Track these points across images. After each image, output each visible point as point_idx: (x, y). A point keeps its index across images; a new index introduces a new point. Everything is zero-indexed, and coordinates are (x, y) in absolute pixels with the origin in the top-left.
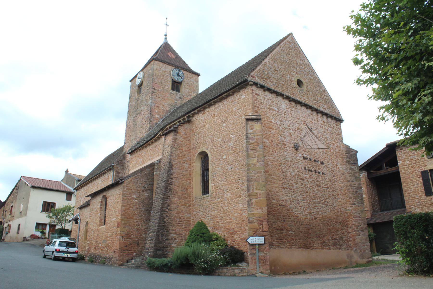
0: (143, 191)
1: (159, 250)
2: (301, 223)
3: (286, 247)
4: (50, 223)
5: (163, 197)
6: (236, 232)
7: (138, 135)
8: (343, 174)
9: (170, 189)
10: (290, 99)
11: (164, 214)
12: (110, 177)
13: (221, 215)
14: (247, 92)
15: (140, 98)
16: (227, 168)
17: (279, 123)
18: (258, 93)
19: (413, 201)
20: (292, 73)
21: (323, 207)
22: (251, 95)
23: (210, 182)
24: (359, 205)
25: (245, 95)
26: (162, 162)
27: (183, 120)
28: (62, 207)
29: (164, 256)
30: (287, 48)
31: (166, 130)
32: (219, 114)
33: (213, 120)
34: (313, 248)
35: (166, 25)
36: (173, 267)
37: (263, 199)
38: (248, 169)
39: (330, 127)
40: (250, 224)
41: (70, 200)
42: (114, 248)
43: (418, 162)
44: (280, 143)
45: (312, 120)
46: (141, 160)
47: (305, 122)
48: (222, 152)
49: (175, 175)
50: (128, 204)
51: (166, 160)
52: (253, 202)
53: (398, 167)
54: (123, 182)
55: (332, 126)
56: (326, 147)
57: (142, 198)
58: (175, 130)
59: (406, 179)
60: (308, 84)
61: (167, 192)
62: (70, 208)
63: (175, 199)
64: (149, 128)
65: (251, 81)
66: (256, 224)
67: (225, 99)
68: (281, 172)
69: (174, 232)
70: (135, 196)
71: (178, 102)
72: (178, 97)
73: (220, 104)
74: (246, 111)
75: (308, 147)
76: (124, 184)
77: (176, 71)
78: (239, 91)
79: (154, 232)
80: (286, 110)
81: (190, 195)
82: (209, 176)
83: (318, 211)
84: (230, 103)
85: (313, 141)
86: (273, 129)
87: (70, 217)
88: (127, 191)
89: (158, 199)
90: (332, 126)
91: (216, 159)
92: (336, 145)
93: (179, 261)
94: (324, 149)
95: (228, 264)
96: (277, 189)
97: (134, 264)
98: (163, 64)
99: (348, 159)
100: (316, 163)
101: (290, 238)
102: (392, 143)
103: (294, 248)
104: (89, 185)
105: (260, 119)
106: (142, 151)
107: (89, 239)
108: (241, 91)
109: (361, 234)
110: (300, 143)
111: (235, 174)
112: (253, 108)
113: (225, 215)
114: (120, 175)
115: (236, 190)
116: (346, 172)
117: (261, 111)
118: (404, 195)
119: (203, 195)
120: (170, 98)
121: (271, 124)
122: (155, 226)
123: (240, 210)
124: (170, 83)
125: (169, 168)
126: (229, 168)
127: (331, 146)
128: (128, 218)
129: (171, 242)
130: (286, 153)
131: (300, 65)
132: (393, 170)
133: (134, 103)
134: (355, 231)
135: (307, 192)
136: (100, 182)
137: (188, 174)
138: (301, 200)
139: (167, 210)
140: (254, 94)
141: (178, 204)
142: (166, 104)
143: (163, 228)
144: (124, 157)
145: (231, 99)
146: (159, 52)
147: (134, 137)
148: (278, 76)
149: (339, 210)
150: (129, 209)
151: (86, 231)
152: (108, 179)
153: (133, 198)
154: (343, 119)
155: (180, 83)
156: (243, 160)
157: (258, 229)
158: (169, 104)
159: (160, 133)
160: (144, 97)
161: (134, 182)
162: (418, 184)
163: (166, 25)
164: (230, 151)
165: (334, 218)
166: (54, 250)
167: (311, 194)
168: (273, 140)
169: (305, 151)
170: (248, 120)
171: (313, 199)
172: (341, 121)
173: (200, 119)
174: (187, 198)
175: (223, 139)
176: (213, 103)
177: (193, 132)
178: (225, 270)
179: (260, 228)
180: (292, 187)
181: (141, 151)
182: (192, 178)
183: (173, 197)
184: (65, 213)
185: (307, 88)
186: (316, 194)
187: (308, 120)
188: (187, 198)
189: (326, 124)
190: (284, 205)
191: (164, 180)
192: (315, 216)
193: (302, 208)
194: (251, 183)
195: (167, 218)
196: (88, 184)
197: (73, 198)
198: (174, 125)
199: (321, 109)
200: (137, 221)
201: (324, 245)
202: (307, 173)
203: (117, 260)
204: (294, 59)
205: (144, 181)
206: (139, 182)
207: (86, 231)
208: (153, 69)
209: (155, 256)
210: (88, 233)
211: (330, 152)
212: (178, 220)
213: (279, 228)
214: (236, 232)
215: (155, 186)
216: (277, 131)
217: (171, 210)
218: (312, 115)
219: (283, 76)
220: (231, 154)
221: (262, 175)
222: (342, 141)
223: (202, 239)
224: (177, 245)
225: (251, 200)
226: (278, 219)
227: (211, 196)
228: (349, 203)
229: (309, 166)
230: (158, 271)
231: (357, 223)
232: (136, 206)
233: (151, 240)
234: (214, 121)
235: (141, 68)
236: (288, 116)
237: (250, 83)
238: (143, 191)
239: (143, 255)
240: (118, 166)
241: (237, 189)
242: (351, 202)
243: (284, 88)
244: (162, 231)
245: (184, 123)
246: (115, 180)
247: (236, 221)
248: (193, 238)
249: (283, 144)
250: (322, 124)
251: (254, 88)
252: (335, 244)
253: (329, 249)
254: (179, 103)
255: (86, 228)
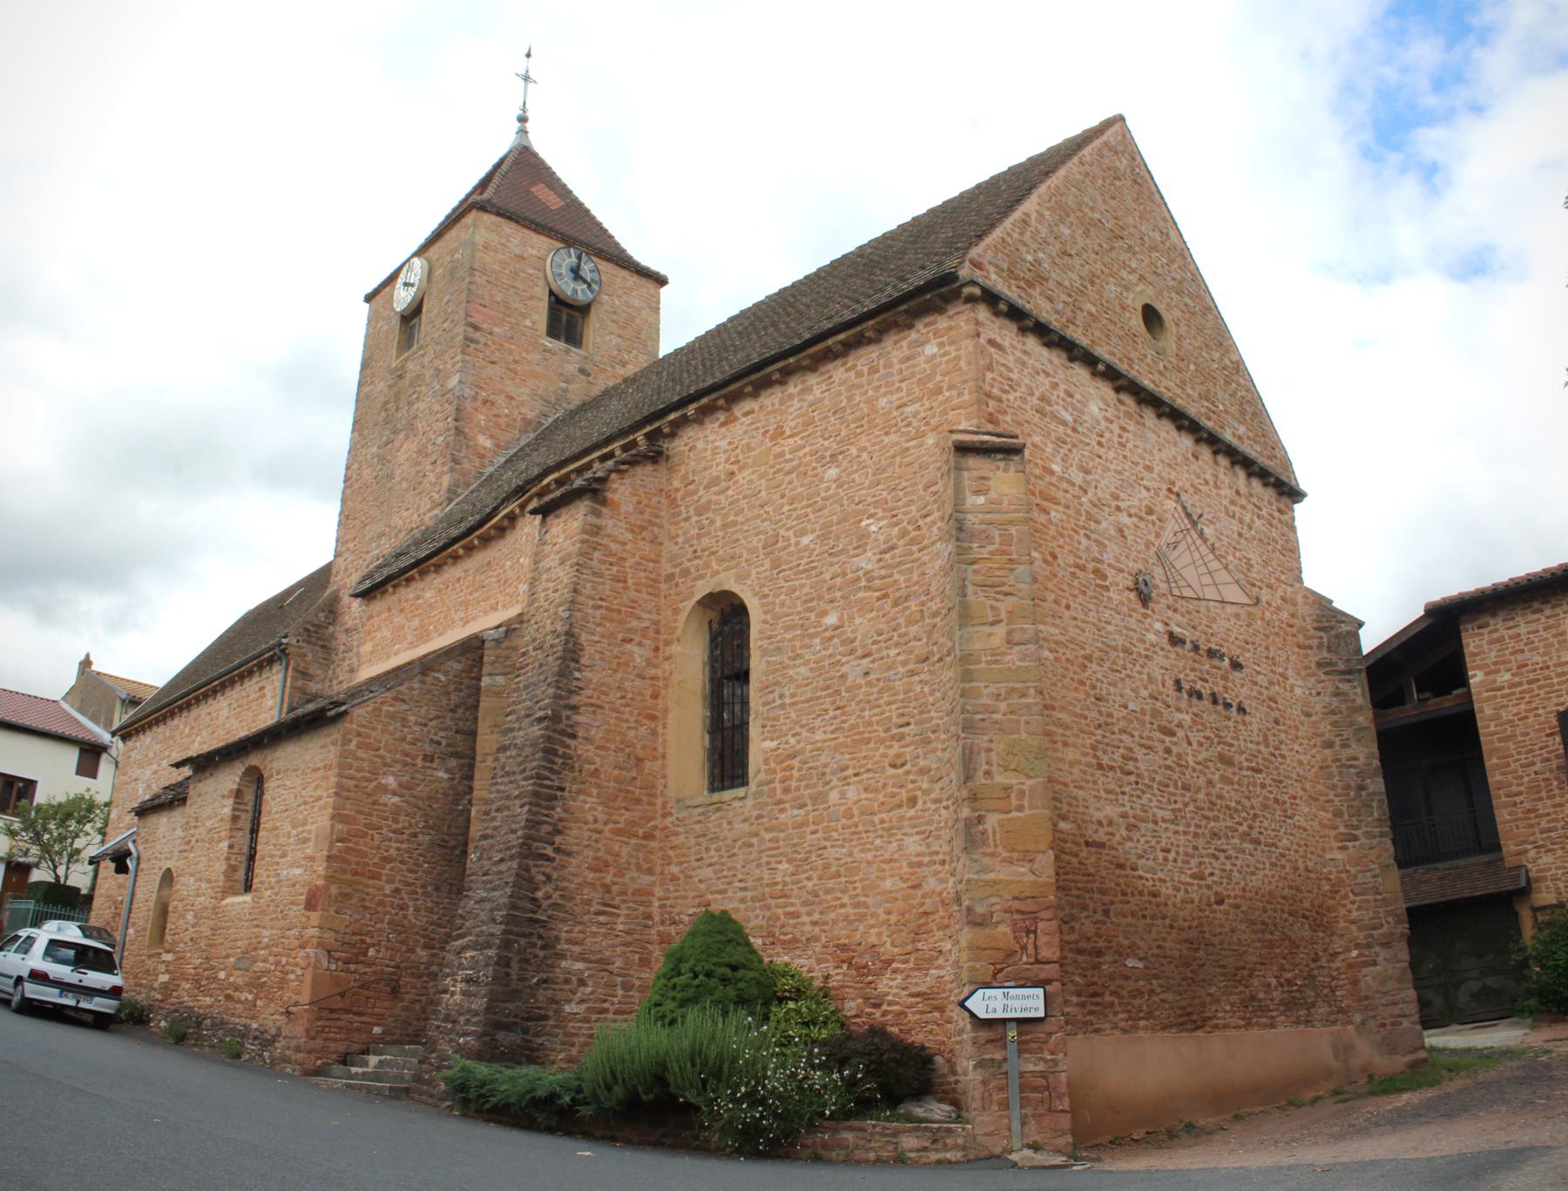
0: (428, 758)
1: (507, 1027)
2: (1167, 922)
3: (1115, 1027)
4: (10, 855)
5: (535, 794)
6: (889, 963)
7: (396, 521)
8: (1308, 715)
9: (566, 756)
10: (1122, 382)
11: (534, 870)
12: (268, 692)
13: (810, 884)
14: (950, 328)
15: (410, 366)
16: (844, 669)
17: (1078, 478)
18: (999, 340)
19: (1531, 826)
20: (1124, 274)
21: (1243, 851)
22: (968, 344)
23: (754, 731)
24: (1375, 841)
25: (941, 345)
26: (530, 631)
27: (625, 448)
28: (62, 798)
29: (529, 1054)
30: (1099, 173)
31: (540, 495)
32: (807, 424)
33: (777, 449)
34: (1216, 1027)
35: (526, 78)
36: (586, 1111)
37: (1034, 812)
38: (967, 676)
39: (1259, 517)
40: (978, 930)
41: (94, 775)
42: (289, 995)
43: (1546, 678)
44: (1082, 568)
45: (1196, 481)
46: (416, 622)
47: (1173, 484)
48: (820, 598)
49: (589, 692)
50: (358, 812)
51: (548, 624)
52: (988, 826)
53: (1469, 694)
54: (345, 713)
55: (1264, 513)
56: (1245, 600)
57: (422, 790)
58: (595, 491)
59: (1500, 740)
60: (1183, 329)
61: (551, 770)
62: (91, 807)
63: (588, 805)
64: (449, 491)
65: (973, 283)
66: (1004, 929)
67: (836, 356)
68: (1088, 695)
69: (576, 949)
70: (391, 781)
71: (571, 387)
72: (572, 368)
73: (812, 379)
74: (944, 412)
75: (1187, 593)
76: (347, 725)
77: (568, 259)
78: (910, 327)
79: (488, 946)
80: (1104, 424)
81: (650, 789)
82: (752, 704)
83: (1228, 867)
84: (859, 374)
85: (1203, 570)
86: (1056, 502)
87: (90, 844)
88: (360, 753)
89: (508, 798)
90: (1264, 513)
91: (788, 628)
92: (1280, 593)
93: (618, 1090)
94: (1243, 605)
95: (861, 1106)
96: (1076, 770)
97: (376, 1077)
98: (513, 225)
99: (1325, 654)
100: (1216, 662)
101: (1130, 985)
102: (1451, 599)
103: (1146, 1028)
104: (176, 721)
105: (1016, 451)
106: (421, 585)
107: (174, 943)
108: (919, 325)
109: (1380, 959)
110: (1158, 572)
111: (886, 698)
112: (978, 402)
113: (830, 884)
114: (314, 687)
115: (892, 771)
116: (1319, 707)
117: (1008, 418)
118: (1494, 802)
119: (712, 790)
120: (538, 369)
121: (1048, 478)
122: (494, 920)
123: (910, 865)
124: (543, 306)
125: (563, 658)
126: (853, 669)
127: (1265, 595)
128: (356, 873)
129: (560, 996)
130: (1107, 614)
131: (1153, 248)
132: (1446, 704)
133: (381, 386)
134: (1357, 946)
135: (1186, 787)
136: (225, 713)
137: (648, 693)
138: (1164, 821)
139: (549, 851)
140: (982, 340)
141: (599, 826)
142: (523, 393)
143: (528, 933)
144: (332, 609)
145: (865, 357)
146: (496, 180)
147: (379, 527)
148: (1075, 277)
149: (1301, 865)
150: (364, 835)
151: (163, 912)
152: (260, 703)
153: (384, 789)
154: (1303, 485)
155: (585, 309)
156: (929, 634)
157: (1011, 954)
158: (533, 394)
159: (513, 506)
160: (427, 359)
161: (392, 716)
162: (1548, 760)
163: (526, 78)
164: (861, 595)
165: (1284, 898)
166: (25, 974)
167: (1201, 796)
168: (1057, 551)
169: (1175, 611)
170: (963, 449)
171: (1207, 818)
172: (1295, 495)
173: (707, 446)
174: (638, 801)
175: (824, 537)
176: (776, 376)
177: (673, 502)
178: (849, 1136)
179: (1024, 948)
180: (1130, 766)
181: (414, 585)
182: (666, 711)
183: (579, 792)
184: (73, 825)
185: (1179, 347)
186: (1220, 797)
187: (1183, 481)
188: (638, 801)
189: (1244, 502)
190: (1102, 845)
191: (541, 714)
192: (1220, 889)
193: (1171, 856)
194: (982, 741)
195: (549, 888)
196: (172, 714)
197: (105, 767)
198: (579, 471)
199: (1227, 436)
200: (397, 891)
201: (1253, 1011)
202: (1183, 705)
203: (298, 1050)
204: (1131, 220)
205: (433, 714)
206: (412, 718)
207: (163, 912)
208: (474, 245)
209: (489, 1052)
210: (172, 917)
211: (1262, 619)
212: (597, 896)
213: (1088, 946)
214: (889, 963)
215: (487, 740)
216: (1070, 512)
217: (569, 854)
218: (1197, 458)
219: (1092, 283)
220: (864, 608)
221: (1028, 706)
222: (1300, 580)
223: (731, 992)
224: (588, 1009)
225: (980, 820)
226: (1085, 908)
227: (757, 795)
228: (1333, 833)
229: (1192, 677)
230: (500, 1123)
231: (1366, 915)
232: (396, 821)
233: (468, 980)
234: (782, 454)
235: (415, 248)
236: (1111, 454)
237: (967, 290)
238: (428, 758)
239: (431, 1046)
240: (307, 648)
241: (894, 766)
242: (1342, 829)
243: (1097, 333)
244: (523, 941)
245: (633, 463)
246: (292, 709)
247: (889, 913)
248: (687, 986)
249: (1096, 571)
250: (1233, 503)
251: (983, 313)
252: (1289, 1005)
253: (1272, 1026)
254: (578, 392)
255: (159, 897)
